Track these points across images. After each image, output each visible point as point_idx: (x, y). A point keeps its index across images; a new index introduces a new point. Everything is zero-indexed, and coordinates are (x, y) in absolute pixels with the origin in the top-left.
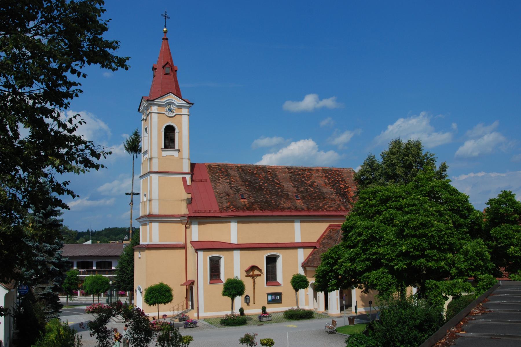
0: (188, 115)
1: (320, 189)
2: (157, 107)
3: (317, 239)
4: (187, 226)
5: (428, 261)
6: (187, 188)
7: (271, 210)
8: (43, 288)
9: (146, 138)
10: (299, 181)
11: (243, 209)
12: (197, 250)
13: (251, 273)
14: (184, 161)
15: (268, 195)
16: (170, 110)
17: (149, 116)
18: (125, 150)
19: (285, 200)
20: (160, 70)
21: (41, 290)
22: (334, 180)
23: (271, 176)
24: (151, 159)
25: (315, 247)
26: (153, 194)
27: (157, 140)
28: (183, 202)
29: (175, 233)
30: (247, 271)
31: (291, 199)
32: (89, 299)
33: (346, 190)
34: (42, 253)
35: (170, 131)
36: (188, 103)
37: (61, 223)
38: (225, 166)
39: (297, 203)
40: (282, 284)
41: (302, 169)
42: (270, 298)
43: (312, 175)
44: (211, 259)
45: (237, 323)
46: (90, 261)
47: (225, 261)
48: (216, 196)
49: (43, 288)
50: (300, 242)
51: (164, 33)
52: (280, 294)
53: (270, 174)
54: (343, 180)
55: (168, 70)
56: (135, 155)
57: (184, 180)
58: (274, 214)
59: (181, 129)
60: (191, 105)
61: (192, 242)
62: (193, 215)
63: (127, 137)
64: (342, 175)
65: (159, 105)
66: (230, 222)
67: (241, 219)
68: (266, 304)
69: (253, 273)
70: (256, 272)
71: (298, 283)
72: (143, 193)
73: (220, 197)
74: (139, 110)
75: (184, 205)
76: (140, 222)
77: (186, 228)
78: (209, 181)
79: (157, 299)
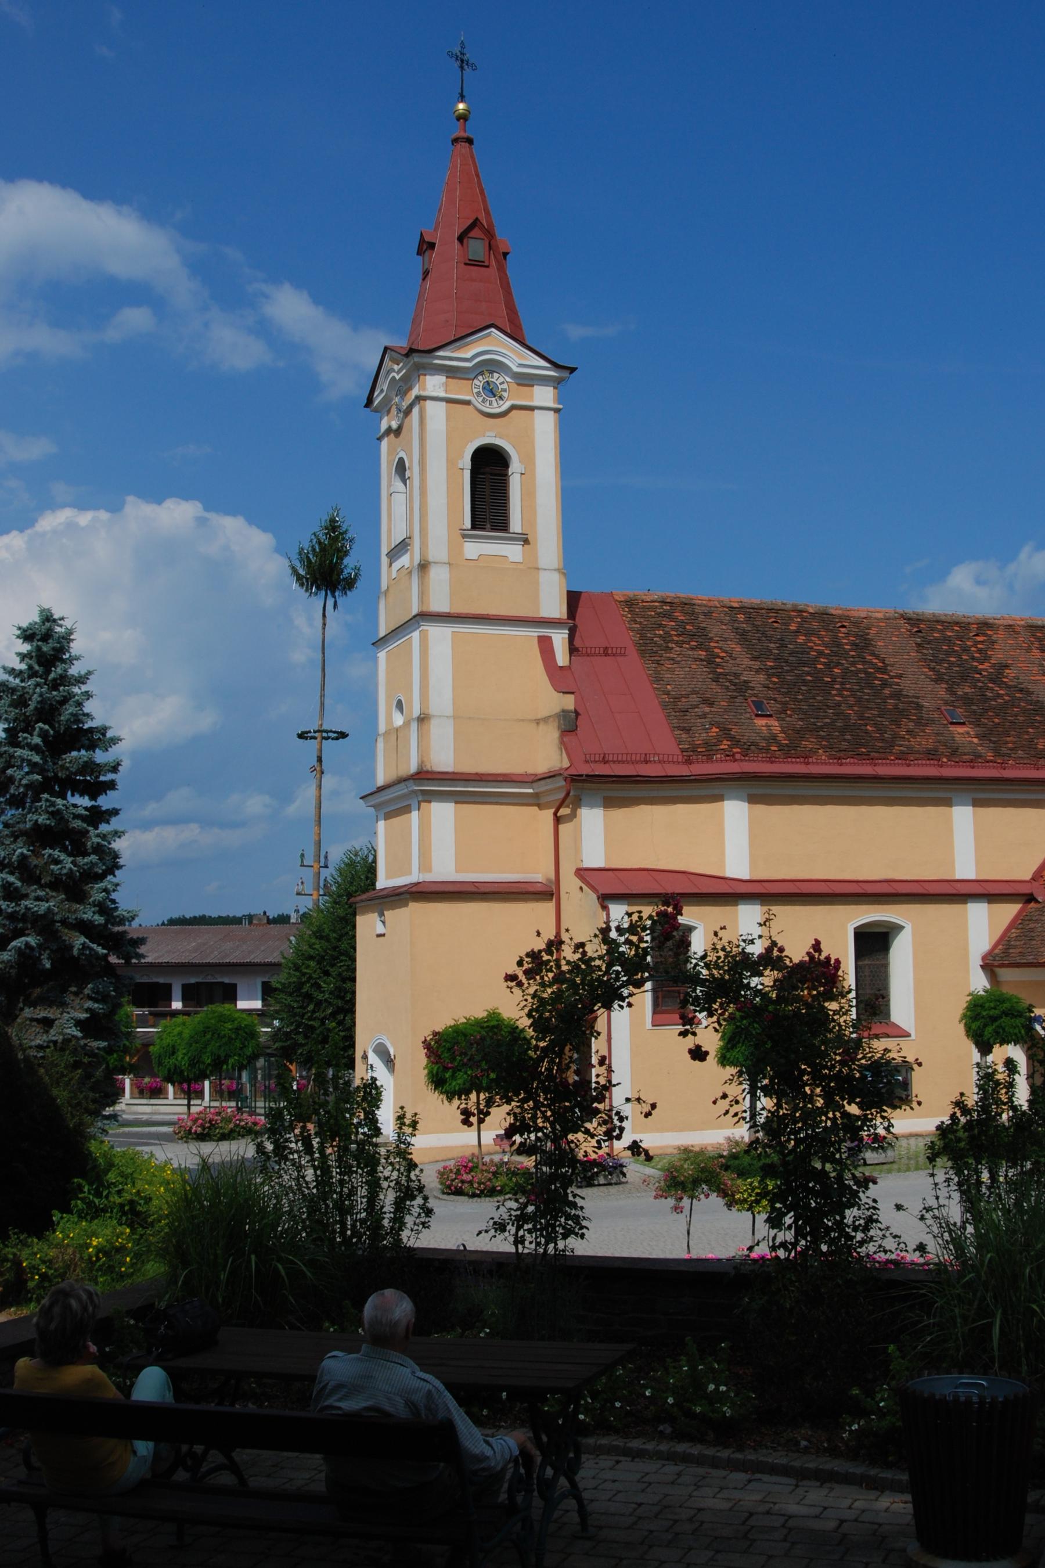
0: (557, 411)
1: (1029, 693)
2: (441, 379)
3: (1034, 868)
4: (564, 811)
7: (867, 758)
8: (47, 1023)
9: (399, 500)
10: (952, 664)
11: (768, 750)
15: (851, 707)
16: (491, 391)
17: (416, 410)
18: (295, 585)
19: (911, 725)
20: (449, 250)
21: (37, 1028)
23: (853, 644)
24: (424, 566)
25: (1030, 898)
28: (542, 726)
29: (517, 842)
31: (932, 721)
32: (163, 1109)
34: (42, 887)
35: (489, 468)
36: (556, 366)
37: (110, 776)
38: (686, 605)
39: (958, 738)
41: (957, 623)
43: (994, 642)
46: (161, 980)
48: (664, 706)
49: (47, 1023)
50: (973, 877)
51: (458, 118)
55: (477, 248)
57: (545, 645)
58: (882, 770)
59: (529, 460)
60: (565, 374)
61: (582, 873)
62: (585, 770)
63: (306, 533)
65: (451, 373)
67: (764, 788)
71: (994, 1019)
72: (388, 697)
73: (677, 709)
75: (551, 735)
77: (558, 820)
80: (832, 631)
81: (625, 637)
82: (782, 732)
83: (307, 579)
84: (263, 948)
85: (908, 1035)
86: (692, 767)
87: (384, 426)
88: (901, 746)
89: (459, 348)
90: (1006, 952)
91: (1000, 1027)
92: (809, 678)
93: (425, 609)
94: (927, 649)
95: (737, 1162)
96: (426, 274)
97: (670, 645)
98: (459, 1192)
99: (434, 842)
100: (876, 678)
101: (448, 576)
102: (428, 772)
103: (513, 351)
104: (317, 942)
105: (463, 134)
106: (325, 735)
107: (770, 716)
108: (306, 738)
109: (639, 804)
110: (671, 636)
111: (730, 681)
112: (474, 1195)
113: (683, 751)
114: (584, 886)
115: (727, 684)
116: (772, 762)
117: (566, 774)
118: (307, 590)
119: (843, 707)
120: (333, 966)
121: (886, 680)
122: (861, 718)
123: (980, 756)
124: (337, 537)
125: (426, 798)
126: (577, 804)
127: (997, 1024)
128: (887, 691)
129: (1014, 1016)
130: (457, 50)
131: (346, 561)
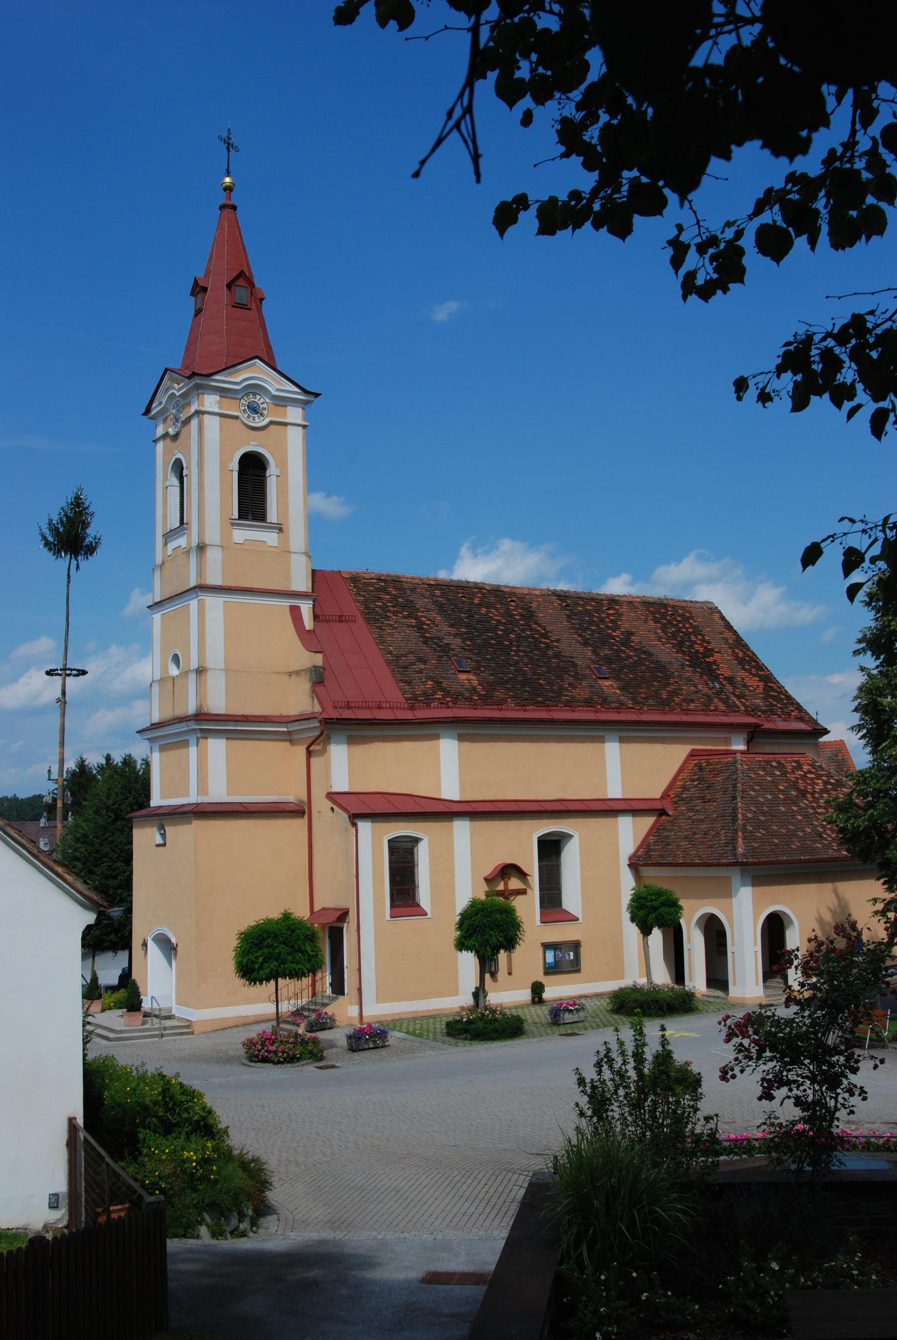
0: (304, 427)
1: (650, 655)
6: (307, 638)
7: (543, 705)
12: (355, 818)
13: (501, 887)
14: (294, 557)
15: (526, 665)
16: (254, 409)
17: (194, 422)
20: (218, 295)
22: (679, 631)
23: (521, 615)
24: (201, 548)
25: (662, 813)
26: (209, 652)
27: (217, 495)
28: (293, 678)
29: (276, 770)
31: (585, 677)
33: (710, 659)
35: (252, 469)
36: (305, 391)
38: (396, 581)
40: (580, 917)
41: (593, 600)
42: (550, 956)
43: (621, 615)
44: (394, 844)
45: (504, 1030)
47: (432, 851)
48: (388, 663)
50: (620, 797)
51: (226, 189)
52: (576, 946)
53: (517, 607)
54: (697, 631)
56: (74, 563)
57: (295, 612)
59: (283, 465)
60: (311, 398)
61: (331, 796)
62: (335, 715)
63: (54, 509)
65: (224, 393)
66: (437, 737)
67: (470, 728)
68: (540, 977)
69: (506, 885)
70: (514, 883)
71: (655, 909)
72: (163, 651)
73: (399, 665)
74: (148, 411)
75: (304, 685)
76: (149, 739)
77: (309, 754)
78: (360, 619)
79: (284, 962)
80: (505, 604)
81: (353, 608)
82: (480, 684)
83: (55, 545)
85: (577, 919)
86: (415, 712)
87: (160, 431)
88: (566, 696)
89: (231, 374)
90: (648, 853)
91: (660, 914)
93: (202, 583)
94: (574, 619)
95: (474, 1026)
96: (198, 312)
97: (388, 614)
98: (265, 1060)
99: (212, 770)
101: (221, 556)
102: (205, 714)
103: (273, 378)
104: (82, 846)
105: (228, 202)
106: (68, 672)
107: (469, 672)
108: (52, 675)
109: (374, 742)
111: (436, 644)
112: (279, 1062)
113: (407, 699)
114: (336, 808)
116: (475, 709)
117: (320, 718)
118: (54, 554)
119: (521, 665)
120: (96, 866)
121: (548, 644)
122: (535, 673)
123: (623, 704)
124: (81, 511)
125: (204, 735)
126: (328, 741)
127: (657, 912)
128: (550, 653)
129: (670, 906)
130: (225, 135)
131: (88, 531)
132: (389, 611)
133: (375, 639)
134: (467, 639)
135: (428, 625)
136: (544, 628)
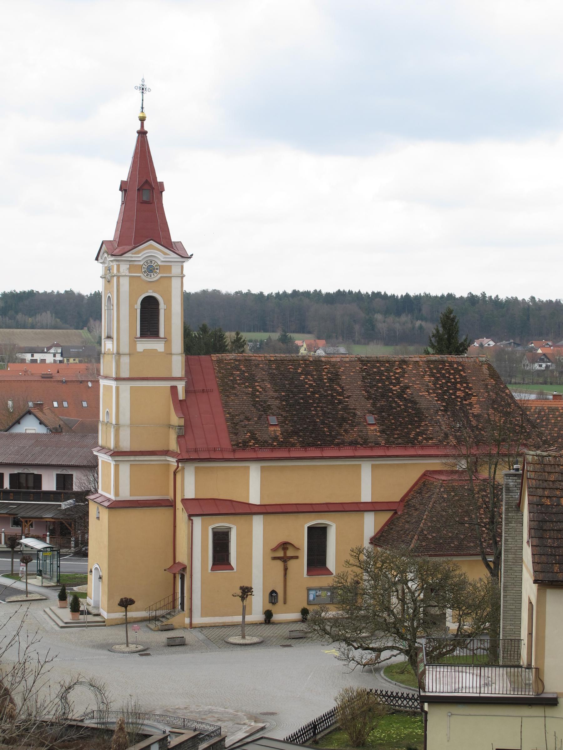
1: (415, 403)
5: (440, 653)
10: (379, 388)
15: (318, 417)
30: (274, 550)
48: (227, 420)
54: (464, 380)
61: (184, 501)
64: (463, 370)
82: (282, 434)
84: (57, 453)
92: (302, 401)
100: (336, 399)
110: (236, 380)
113: (232, 445)
115: (260, 407)
132: (237, 383)
133: (223, 403)
134: (283, 400)
135: (260, 392)
136: (342, 388)
